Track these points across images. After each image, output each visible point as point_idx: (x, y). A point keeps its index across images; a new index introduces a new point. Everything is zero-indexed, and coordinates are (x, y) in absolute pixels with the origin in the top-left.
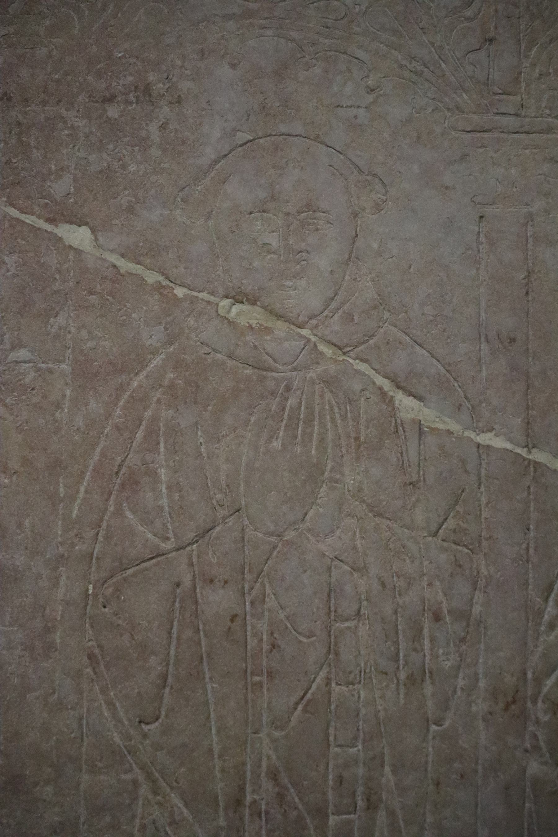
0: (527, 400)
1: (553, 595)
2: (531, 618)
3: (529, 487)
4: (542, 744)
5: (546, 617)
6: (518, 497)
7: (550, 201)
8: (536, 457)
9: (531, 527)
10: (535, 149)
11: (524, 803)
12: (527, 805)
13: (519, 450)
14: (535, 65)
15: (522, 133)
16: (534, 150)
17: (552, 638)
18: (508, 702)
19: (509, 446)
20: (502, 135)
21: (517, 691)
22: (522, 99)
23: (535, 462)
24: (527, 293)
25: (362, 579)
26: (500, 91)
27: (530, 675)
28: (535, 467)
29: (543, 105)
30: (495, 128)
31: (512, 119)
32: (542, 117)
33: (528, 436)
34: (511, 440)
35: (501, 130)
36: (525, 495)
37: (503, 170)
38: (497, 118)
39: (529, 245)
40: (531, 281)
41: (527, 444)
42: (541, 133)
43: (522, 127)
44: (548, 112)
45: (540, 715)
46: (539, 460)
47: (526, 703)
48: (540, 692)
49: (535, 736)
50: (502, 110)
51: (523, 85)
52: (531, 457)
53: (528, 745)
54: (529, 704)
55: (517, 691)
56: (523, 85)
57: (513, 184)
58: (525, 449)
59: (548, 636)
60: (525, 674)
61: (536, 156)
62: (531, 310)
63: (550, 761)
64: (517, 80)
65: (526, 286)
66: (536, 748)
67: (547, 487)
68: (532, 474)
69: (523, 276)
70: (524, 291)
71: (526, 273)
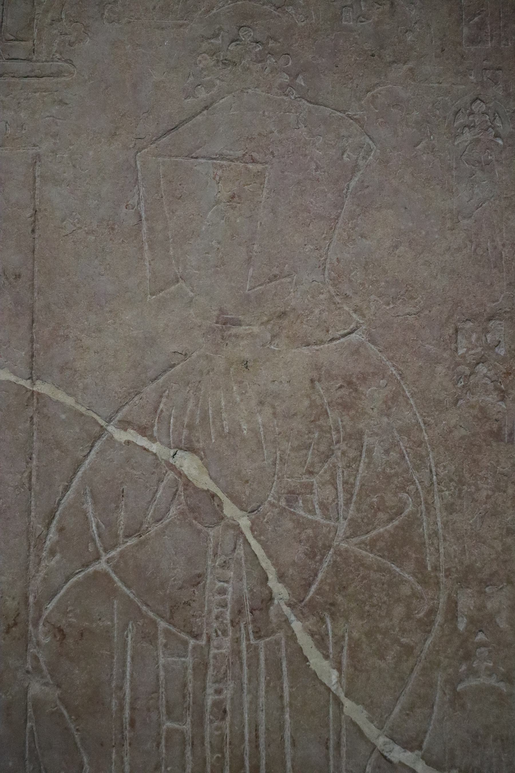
0: (32, 333)
1: (55, 522)
2: (33, 543)
3: (32, 418)
4: (44, 667)
5: (48, 542)
6: (20, 427)
7: (58, 141)
8: (39, 388)
9: (34, 456)
10: (45, 92)
11: (26, 721)
12: (29, 724)
13: (22, 382)
14: (48, 12)
15: (33, 77)
16: (44, 93)
17: (53, 563)
18: (9, 625)
19: (13, 378)
20: (13, 80)
21: (18, 615)
22: (34, 45)
23: (39, 394)
24: (33, 231)
25: (399, 631)
26: (12, 38)
27: (31, 599)
28: (38, 399)
29: (55, 49)
30: (6, 73)
31: (24, 63)
32: (52, 61)
33: (32, 369)
34: (14, 373)
35: (12, 75)
36: (28, 424)
37: (13, 113)
38: (9, 63)
39: (37, 184)
40: (38, 219)
41: (30, 376)
42: (51, 76)
43: (32, 71)
44: (58, 55)
45: (41, 637)
46: (42, 392)
47: (27, 626)
48: (40, 616)
49: (36, 658)
50: (13, 56)
51: (36, 31)
52: (35, 389)
53: (29, 666)
54: (30, 627)
55: (18, 615)
56: (36, 31)
57: (22, 126)
58: (29, 381)
59: (49, 562)
60: (27, 598)
61: (46, 99)
62: (37, 247)
63: (51, 682)
64: (29, 26)
65: (32, 224)
66: (37, 669)
67: (49, 417)
68: (35, 404)
69: (29, 215)
70: (30, 230)
71: (32, 212)
